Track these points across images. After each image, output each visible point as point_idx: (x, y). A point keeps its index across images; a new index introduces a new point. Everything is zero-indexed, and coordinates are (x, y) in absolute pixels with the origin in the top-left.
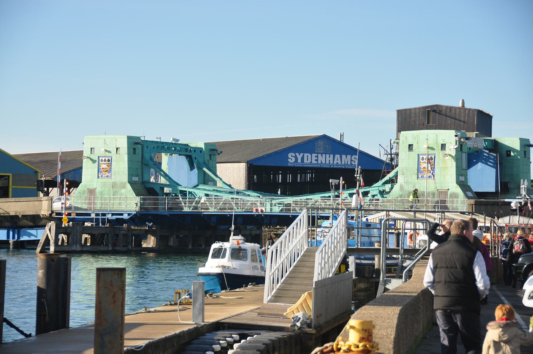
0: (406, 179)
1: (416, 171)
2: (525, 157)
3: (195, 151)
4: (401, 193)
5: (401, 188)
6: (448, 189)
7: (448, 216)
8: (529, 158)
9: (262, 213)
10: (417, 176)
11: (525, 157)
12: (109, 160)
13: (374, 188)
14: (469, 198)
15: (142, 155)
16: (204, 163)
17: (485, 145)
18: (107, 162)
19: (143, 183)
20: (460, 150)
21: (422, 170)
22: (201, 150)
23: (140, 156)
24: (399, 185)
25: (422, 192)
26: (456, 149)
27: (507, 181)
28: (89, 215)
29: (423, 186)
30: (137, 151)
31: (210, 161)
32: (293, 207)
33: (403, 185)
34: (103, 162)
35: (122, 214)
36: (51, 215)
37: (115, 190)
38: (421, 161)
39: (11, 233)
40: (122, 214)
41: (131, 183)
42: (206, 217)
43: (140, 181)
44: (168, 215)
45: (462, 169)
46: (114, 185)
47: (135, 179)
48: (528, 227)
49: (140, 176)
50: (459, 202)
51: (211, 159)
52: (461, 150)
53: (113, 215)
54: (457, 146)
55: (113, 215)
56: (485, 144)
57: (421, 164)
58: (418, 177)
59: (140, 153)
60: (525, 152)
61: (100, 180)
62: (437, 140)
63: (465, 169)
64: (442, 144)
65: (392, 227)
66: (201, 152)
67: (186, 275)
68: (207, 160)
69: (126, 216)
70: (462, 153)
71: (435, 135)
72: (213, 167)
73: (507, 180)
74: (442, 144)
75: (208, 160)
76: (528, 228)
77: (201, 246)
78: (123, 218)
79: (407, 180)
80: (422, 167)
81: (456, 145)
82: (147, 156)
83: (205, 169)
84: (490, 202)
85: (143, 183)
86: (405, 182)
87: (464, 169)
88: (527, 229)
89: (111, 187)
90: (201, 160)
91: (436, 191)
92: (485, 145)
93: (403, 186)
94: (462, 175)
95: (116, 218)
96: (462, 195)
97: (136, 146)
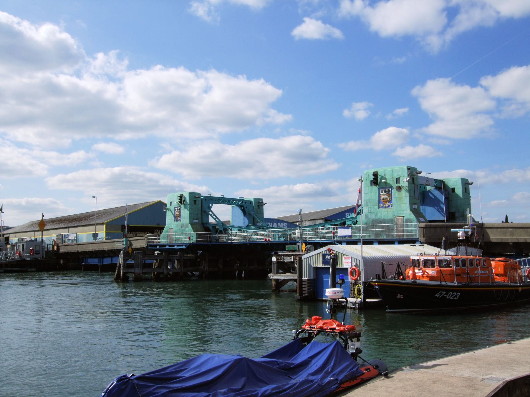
2: (466, 192)
3: (246, 203)
5: (366, 216)
7: (153, 201)
8: (469, 194)
10: (378, 206)
11: (466, 192)
12: (179, 210)
15: (202, 205)
18: (178, 211)
19: (203, 224)
21: (382, 201)
22: (250, 202)
23: (200, 206)
25: (382, 220)
26: (408, 181)
27: (453, 211)
30: (197, 202)
34: (177, 211)
35: (182, 246)
36: (147, 247)
37: (183, 229)
38: (381, 194)
39: (100, 259)
41: (192, 223)
43: (200, 222)
44: (210, 245)
45: (415, 199)
46: (182, 226)
49: (200, 220)
50: (413, 226)
51: (259, 209)
52: (413, 182)
54: (409, 179)
57: (381, 196)
58: (379, 207)
59: (200, 204)
60: (466, 188)
62: (393, 175)
63: (418, 198)
64: (397, 178)
65: (197, 260)
67: (52, 315)
68: (256, 209)
69: (184, 247)
70: (414, 185)
71: (391, 171)
73: (453, 210)
74: (397, 178)
78: (182, 248)
82: (205, 206)
84: (438, 225)
87: (417, 199)
89: (181, 227)
91: (393, 218)
92: (435, 184)
93: (368, 216)
94: (415, 204)
96: (415, 221)
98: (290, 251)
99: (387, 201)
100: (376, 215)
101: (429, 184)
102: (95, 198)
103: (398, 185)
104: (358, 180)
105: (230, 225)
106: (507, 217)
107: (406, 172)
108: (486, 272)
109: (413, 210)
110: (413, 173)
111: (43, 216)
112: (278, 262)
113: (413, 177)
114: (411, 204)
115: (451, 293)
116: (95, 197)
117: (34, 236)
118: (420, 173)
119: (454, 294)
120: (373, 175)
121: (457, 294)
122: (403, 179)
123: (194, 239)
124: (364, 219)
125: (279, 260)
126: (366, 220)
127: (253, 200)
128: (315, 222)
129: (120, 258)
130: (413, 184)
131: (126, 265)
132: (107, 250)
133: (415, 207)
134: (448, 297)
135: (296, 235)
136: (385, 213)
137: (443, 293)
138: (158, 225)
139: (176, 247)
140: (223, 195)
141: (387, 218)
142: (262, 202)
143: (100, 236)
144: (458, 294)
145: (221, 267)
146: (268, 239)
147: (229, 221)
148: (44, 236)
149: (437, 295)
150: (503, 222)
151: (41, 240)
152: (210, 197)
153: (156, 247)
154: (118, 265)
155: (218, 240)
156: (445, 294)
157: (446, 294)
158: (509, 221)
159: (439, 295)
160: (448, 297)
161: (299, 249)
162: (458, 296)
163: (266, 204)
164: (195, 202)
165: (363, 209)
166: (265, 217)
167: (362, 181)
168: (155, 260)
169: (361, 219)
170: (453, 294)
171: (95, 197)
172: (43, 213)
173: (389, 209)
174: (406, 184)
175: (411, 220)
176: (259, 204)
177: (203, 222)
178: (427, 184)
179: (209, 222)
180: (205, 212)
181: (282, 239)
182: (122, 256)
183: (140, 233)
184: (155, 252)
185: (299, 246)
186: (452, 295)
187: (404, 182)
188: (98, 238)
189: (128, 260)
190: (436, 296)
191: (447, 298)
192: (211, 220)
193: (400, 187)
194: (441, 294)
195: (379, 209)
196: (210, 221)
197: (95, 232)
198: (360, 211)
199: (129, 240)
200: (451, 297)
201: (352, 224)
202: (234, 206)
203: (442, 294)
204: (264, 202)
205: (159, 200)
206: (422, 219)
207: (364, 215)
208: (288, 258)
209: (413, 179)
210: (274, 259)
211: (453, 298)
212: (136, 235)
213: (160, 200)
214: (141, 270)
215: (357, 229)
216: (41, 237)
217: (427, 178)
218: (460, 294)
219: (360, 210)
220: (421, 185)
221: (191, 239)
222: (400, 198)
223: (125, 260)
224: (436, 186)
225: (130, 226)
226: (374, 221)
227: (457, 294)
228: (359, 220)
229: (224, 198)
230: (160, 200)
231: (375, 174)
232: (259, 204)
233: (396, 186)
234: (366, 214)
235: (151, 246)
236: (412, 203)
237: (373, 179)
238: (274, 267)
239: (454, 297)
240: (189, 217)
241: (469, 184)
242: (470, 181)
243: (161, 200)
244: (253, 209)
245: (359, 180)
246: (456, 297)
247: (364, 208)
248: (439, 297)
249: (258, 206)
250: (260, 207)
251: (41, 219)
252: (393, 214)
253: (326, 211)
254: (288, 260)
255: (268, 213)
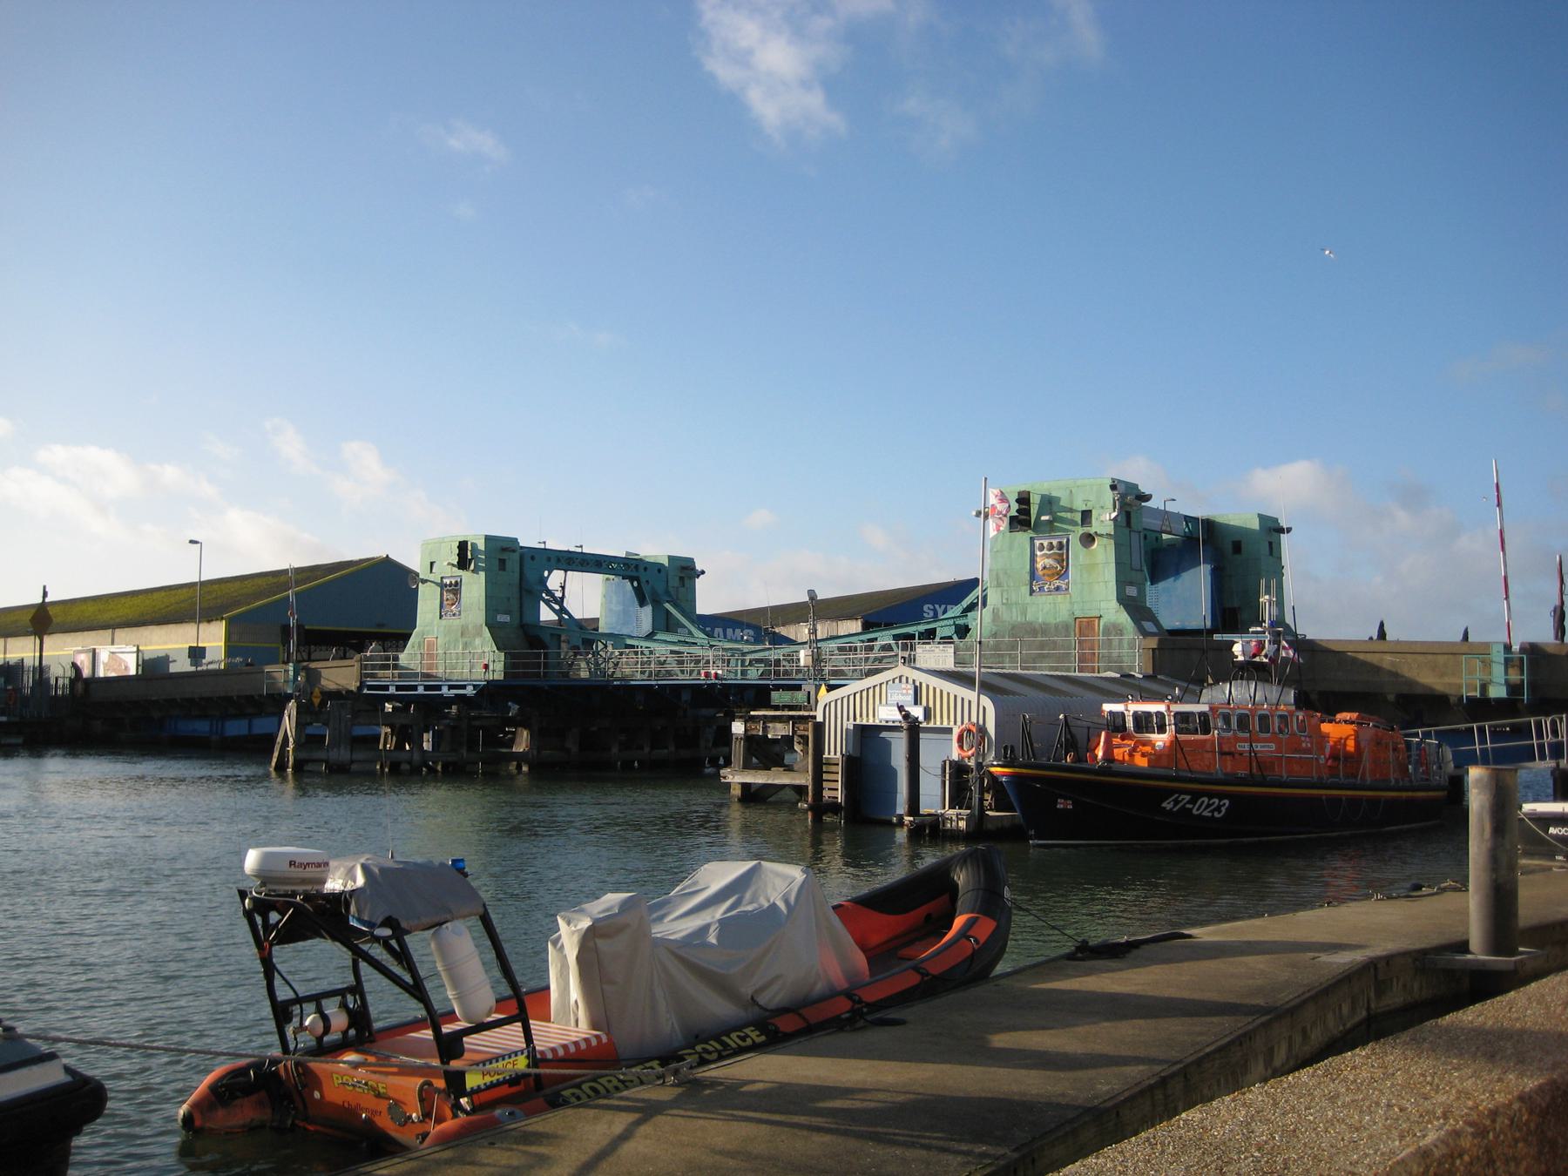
0: (1005, 596)
1: (1028, 577)
2: (1271, 553)
3: (645, 569)
4: (995, 629)
5: (995, 613)
6: (1101, 616)
9: (717, 681)
13: (946, 622)
14: (1145, 633)
16: (667, 592)
17: (1187, 530)
19: (523, 626)
20: (1125, 525)
21: (1041, 573)
22: (659, 568)
23: (517, 575)
24: (991, 610)
25: (1040, 625)
26: (1115, 520)
27: (1236, 604)
28: (386, 688)
29: (1042, 611)
30: (509, 565)
31: (682, 590)
32: (784, 666)
33: (998, 609)
35: (464, 687)
36: (360, 688)
39: (215, 722)
40: (464, 687)
41: (492, 625)
42: (668, 692)
45: (1132, 569)
47: (503, 618)
48: (1280, 713)
51: (684, 586)
52: (1128, 524)
53: (451, 687)
55: (451, 687)
56: (1187, 525)
58: (1032, 592)
59: (517, 569)
60: (1270, 544)
61: (444, 622)
66: (659, 571)
69: (470, 691)
71: (1068, 492)
72: (687, 601)
75: (677, 588)
76: (1281, 717)
77: (642, 748)
79: (1007, 599)
80: (1039, 566)
81: (1114, 511)
82: (531, 576)
83: (667, 606)
85: (523, 626)
86: (1003, 604)
87: (1136, 570)
88: (1276, 720)
89: (460, 634)
90: (660, 588)
91: (1071, 621)
94: (1131, 584)
95: (456, 695)
96: (1132, 630)
97: (504, 556)
98: (784, 707)
99: (1053, 574)
100: (1024, 613)
101: (1168, 529)
102: (199, 545)
103: (1086, 529)
104: (974, 513)
105: (597, 629)
106: (1382, 625)
107: (1109, 497)
108: (1268, 746)
109: (1123, 600)
110: (1130, 500)
111: (45, 594)
112: (749, 738)
113: (1128, 509)
114: (1121, 583)
115: (1206, 799)
116: (196, 542)
117: (5, 653)
118: (1147, 498)
119: (1214, 803)
120: (1017, 501)
121: (1220, 801)
122: (1099, 515)
123: (497, 672)
124: (990, 621)
125: (754, 733)
126: (996, 626)
127: (666, 563)
128: (835, 628)
129: (287, 718)
130: (1129, 529)
131: (303, 740)
132: (238, 697)
133: (1132, 591)
134: (1198, 810)
135: (802, 663)
136: (1049, 609)
137: (1183, 799)
138: (381, 625)
139: (445, 690)
140: (581, 547)
141: (1051, 620)
142: (694, 568)
143: (209, 658)
144: (1224, 804)
145: (574, 749)
146: (713, 672)
147: (597, 620)
148: (10, 653)
149: (1167, 805)
150: (1371, 638)
151: (37, 664)
152: (545, 549)
153: (388, 690)
154: (280, 739)
155: (566, 675)
156: (1188, 802)
157: (1193, 801)
158: (1391, 635)
159: (1172, 803)
160: (1198, 810)
161: (809, 703)
162: (1223, 809)
163: (703, 572)
164: (502, 562)
165: (986, 595)
166: (698, 613)
167: (986, 517)
168: (386, 725)
169: (980, 622)
170: (1211, 802)
171: (196, 542)
172: (44, 587)
173: (1060, 598)
174: (1110, 529)
175: (1121, 628)
176: (686, 571)
177: (524, 622)
178: (1164, 528)
179: (541, 619)
180: (530, 592)
181: (754, 676)
182: (294, 713)
183: (321, 650)
184: (386, 704)
185: (809, 693)
186: (1209, 806)
187: (1105, 519)
188: (204, 661)
189: (311, 724)
190: (1165, 808)
191: (1195, 812)
192: (546, 614)
193: (1090, 535)
194: (1176, 802)
195: (1031, 594)
196: (543, 618)
197: (195, 645)
198: (976, 601)
199: (306, 669)
200: (1205, 809)
201: (955, 637)
202: (612, 577)
203: (1181, 801)
204: (699, 567)
205: (385, 556)
206: (1149, 626)
207: (987, 612)
208: (779, 726)
209: (1128, 515)
210: (738, 728)
211: (1210, 814)
212: (345, 653)
213: (387, 556)
214: (349, 752)
215: (968, 650)
216: (37, 654)
217: (1166, 512)
218: (1230, 806)
219: (978, 597)
220: (1148, 533)
221: (491, 668)
222: (1090, 568)
223: (300, 725)
224: (1187, 535)
225: (307, 627)
226: (1015, 630)
227: (1220, 801)
228: (974, 624)
229: (585, 554)
230: (387, 556)
231: (1023, 499)
232: (686, 571)
233: (1081, 532)
234: (994, 609)
235: (371, 688)
236: (1124, 582)
237: (1017, 511)
238: (738, 750)
239: (1212, 811)
240: (483, 606)
241: (1281, 530)
242: (1284, 524)
243: (390, 556)
244: (667, 586)
245: (978, 514)
246: (1220, 812)
247: (989, 592)
248: (1171, 809)
249: (682, 579)
250: (687, 582)
251: (40, 601)
252: (1069, 611)
253: (593, 555)
254: (778, 731)
255: (710, 599)
